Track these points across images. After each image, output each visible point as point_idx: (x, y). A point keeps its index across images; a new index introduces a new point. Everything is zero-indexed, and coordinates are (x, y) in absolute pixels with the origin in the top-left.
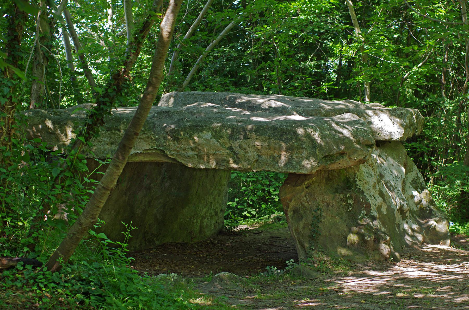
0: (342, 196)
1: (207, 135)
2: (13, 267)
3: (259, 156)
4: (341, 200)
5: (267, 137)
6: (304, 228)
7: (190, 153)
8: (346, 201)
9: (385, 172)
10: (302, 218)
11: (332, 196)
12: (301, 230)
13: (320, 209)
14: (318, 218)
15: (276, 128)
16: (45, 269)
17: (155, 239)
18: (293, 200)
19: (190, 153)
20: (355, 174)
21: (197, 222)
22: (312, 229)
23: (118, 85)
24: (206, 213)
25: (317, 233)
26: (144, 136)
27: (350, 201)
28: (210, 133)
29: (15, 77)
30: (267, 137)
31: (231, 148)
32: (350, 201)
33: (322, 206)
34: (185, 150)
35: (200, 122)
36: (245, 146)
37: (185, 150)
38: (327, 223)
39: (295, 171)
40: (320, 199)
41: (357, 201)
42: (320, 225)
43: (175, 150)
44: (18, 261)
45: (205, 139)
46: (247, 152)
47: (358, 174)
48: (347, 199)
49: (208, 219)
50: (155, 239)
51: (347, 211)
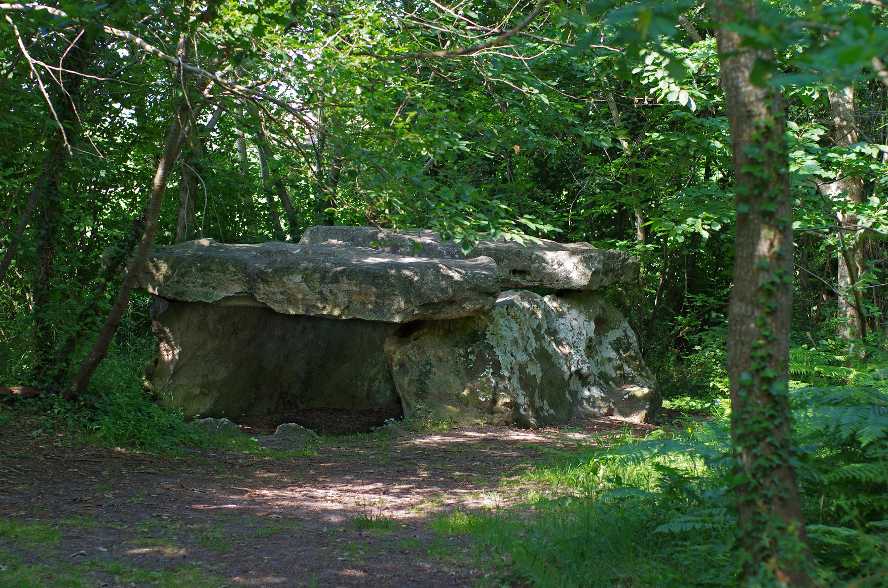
0: (461, 351)
1: (298, 278)
2: (37, 395)
3: (350, 302)
4: (460, 355)
5: (359, 282)
6: (409, 384)
7: (280, 297)
8: (466, 356)
9: (562, 327)
10: (408, 372)
11: (447, 350)
12: (406, 386)
13: (430, 364)
14: (426, 374)
15: (368, 272)
16: (61, 396)
17: (298, 401)
18: (397, 353)
19: (280, 297)
20: (487, 326)
21: (362, 385)
22: (419, 386)
23: (137, 231)
24: (375, 375)
25: (423, 391)
26: (235, 278)
27: (471, 357)
28: (300, 276)
29: (53, 220)
30: (359, 282)
31: (321, 293)
32: (471, 357)
33: (433, 360)
34: (274, 294)
35: (292, 263)
36: (335, 291)
37: (274, 294)
38: (437, 380)
39: (385, 320)
40: (430, 353)
41: (480, 356)
42: (427, 382)
43: (264, 294)
44: (42, 390)
45: (295, 283)
46: (337, 298)
47: (491, 327)
48: (467, 355)
49: (380, 382)
50: (298, 401)
51: (467, 368)
